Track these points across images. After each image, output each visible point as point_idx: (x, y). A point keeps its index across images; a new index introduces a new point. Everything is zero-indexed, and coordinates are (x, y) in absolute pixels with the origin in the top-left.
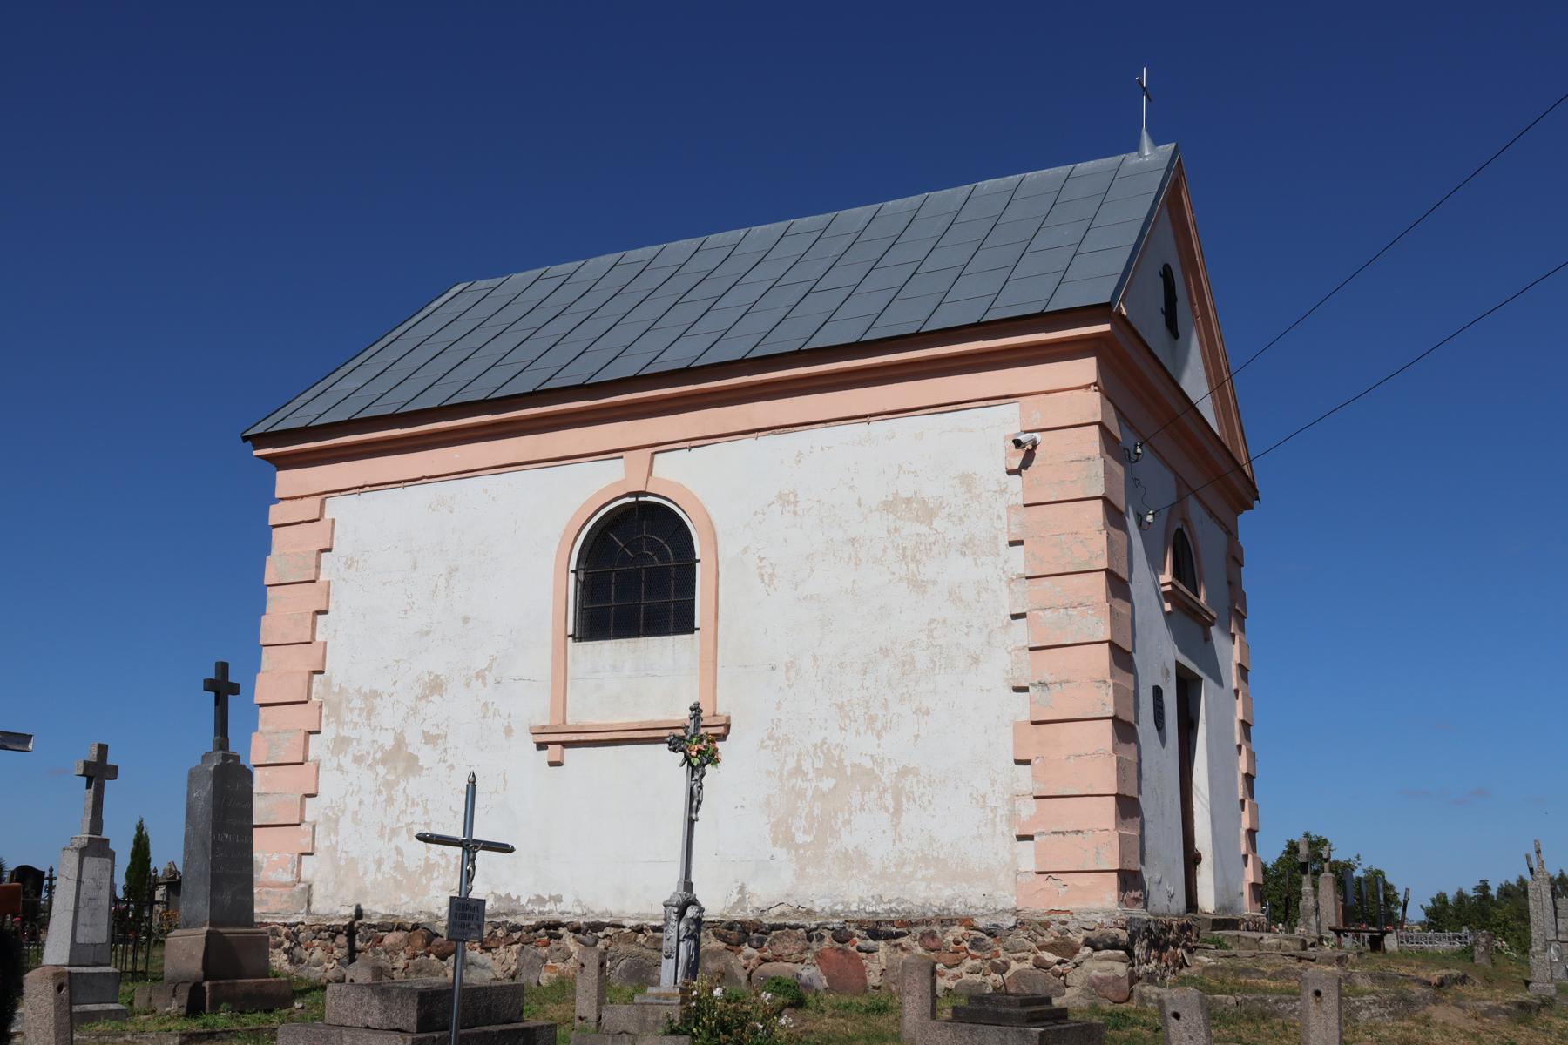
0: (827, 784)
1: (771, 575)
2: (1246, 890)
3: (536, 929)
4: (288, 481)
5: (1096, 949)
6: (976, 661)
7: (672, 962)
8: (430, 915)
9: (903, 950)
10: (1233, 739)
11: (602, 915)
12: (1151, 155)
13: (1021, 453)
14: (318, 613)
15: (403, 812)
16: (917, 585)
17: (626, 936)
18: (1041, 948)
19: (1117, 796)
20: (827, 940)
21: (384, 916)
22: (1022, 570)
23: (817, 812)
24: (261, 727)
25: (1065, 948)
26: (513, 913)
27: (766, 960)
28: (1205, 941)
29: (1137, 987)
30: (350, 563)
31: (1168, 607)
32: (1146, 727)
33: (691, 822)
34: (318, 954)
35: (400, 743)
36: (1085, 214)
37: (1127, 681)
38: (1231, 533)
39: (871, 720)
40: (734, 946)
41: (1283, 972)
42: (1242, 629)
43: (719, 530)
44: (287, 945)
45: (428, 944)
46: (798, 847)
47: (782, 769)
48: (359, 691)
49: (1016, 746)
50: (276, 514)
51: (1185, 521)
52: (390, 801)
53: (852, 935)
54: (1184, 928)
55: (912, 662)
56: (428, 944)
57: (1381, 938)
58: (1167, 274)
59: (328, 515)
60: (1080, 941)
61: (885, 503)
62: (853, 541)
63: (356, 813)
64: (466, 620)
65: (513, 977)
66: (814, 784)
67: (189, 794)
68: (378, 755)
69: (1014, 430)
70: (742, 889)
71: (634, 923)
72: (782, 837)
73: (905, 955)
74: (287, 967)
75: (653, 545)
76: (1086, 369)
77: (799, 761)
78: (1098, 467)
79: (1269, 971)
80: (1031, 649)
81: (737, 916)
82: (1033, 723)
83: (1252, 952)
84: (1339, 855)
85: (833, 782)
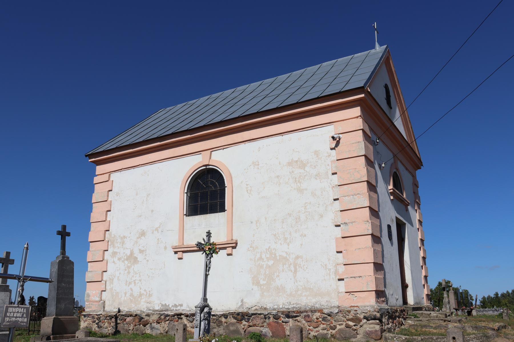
0: (271, 263)
1: (250, 190)
2: (425, 297)
3: (174, 316)
4: (100, 169)
5: (368, 320)
6: (322, 216)
7: (198, 329)
8: (141, 311)
9: (298, 322)
10: (418, 245)
12: (379, 49)
13: (335, 142)
14: (108, 211)
15: (133, 276)
16: (300, 191)
18: (348, 320)
19: (374, 263)
20: (271, 319)
21: (127, 312)
22: (337, 183)
23: (267, 273)
24: (90, 249)
25: (357, 320)
26: (167, 310)
27: (250, 326)
28: (410, 315)
29: (384, 334)
31: (392, 198)
32: (385, 238)
33: (206, 276)
34: (106, 324)
35: (132, 253)
36: (358, 67)
37: (377, 222)
38: (414, 176)
39: (286, 239)
40: (240, 321)
41: (439, 326)
42: (419, 208)
43: (233, 176)
44: (97, 321)
45: (140, 321)
48: (120, 236)
49: (337, 246)
50: (96, 180)
51: (397, 169)
52: (129, 273)
53: (280, 317)
54: (402, 311)
56: (140, 321)
57: (471, 311)
58: (386, 87)
59: (111, 179)
60: (362, 317)
61: (289, 163)
62: (278, 177)
63: (118, 277)
64: (152, 211)
65: (167, 332)
67: (51, 270)
68: (125, 257)
69: (333, 134)
70: (242, 301)
72: (256, 282)
73: (299, 324)
74: (97, 329)
75: (212, 183)
76: (357, 111)
77: (261, 255)
78: (362, 145)
79: (434, 326)
80: (341, 211)
81: (241, 310)
82: (343, 238)
83: (427, 319)
84: (455, 286)
85: (273, 262)
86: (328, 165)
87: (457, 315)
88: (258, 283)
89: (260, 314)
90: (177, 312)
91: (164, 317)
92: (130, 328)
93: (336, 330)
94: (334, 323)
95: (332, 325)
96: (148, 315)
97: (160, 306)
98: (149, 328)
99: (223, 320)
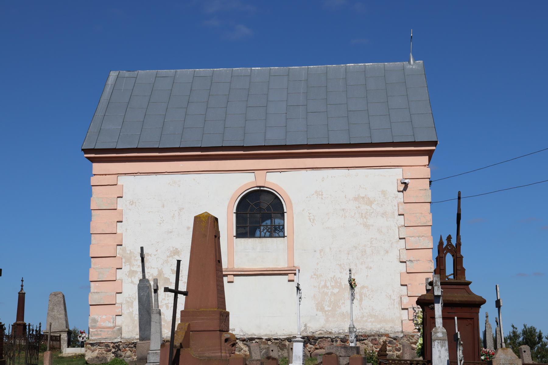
0: (336, 291)
1: (313, 219)
4: (97, 167)
6: (387, 252)
11: (251, 335)
16: (366, 226)
17: (264, 342)
23: (332, 300)
24: (92, 266)
27: (317, 349)
30: (132, 203)
34: (129, 353)
44: (113, 350)
46: (326, 311)
47: (319, 285)
48: (168, 257)
50: (94, 180)
55: (365, 251)
61: (355, 198)
62: (343, 210)
66: (331, 290)
70: (305, 325)
71: (267, 337)
72: (320, 308)
77: (325, 283)
86: (395, 206)
88: (322, 309)
89: (327, 338)
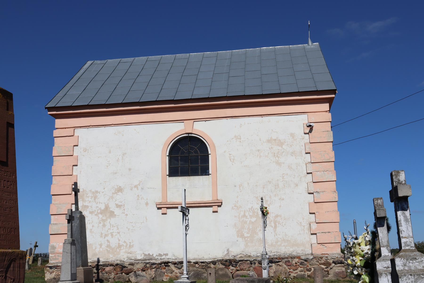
1: (233, 159)
3: (161, 264)
4: (59, 122)
6: (297, 185)
9: (280, 266)
15: (109, 229)
16: (279, 164)
18: (320, 264)
20: (257, 264)
23: (251, 227)
25: (327, 264)
26: (151, 259)
27: (238, 270)
35: (107, 207)
40: (227, 266)
43: (216, 145)
45: (122, 270)
50: (56, 133)
52: (104, 226)
56: (122, 270)
61: (268, 140)
62: (259, 150)
68: (99, 211)
70: (228, 250)
72: (240, 235)
77: (244, 213)
81: (227, 258)
86: (302, 146)
87: (350, 277)
88: (242, 236)
89: (247, 261)
90: (164, 260)
91: (149, 265)
92: (111, 277)
93: (312, 271)
94: (310, 267)
95: (308, 268)
96: (132, 264)
97: (143, 256)
98: (133, 276)
99: (212, 266)
